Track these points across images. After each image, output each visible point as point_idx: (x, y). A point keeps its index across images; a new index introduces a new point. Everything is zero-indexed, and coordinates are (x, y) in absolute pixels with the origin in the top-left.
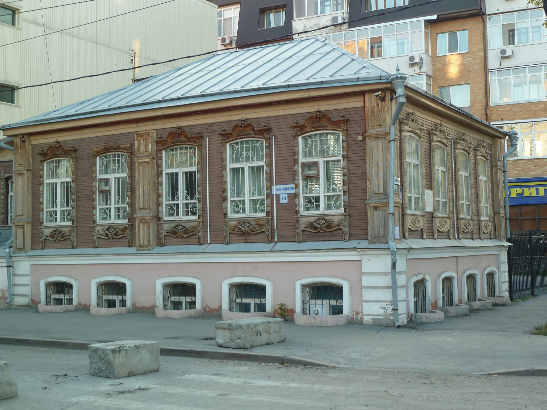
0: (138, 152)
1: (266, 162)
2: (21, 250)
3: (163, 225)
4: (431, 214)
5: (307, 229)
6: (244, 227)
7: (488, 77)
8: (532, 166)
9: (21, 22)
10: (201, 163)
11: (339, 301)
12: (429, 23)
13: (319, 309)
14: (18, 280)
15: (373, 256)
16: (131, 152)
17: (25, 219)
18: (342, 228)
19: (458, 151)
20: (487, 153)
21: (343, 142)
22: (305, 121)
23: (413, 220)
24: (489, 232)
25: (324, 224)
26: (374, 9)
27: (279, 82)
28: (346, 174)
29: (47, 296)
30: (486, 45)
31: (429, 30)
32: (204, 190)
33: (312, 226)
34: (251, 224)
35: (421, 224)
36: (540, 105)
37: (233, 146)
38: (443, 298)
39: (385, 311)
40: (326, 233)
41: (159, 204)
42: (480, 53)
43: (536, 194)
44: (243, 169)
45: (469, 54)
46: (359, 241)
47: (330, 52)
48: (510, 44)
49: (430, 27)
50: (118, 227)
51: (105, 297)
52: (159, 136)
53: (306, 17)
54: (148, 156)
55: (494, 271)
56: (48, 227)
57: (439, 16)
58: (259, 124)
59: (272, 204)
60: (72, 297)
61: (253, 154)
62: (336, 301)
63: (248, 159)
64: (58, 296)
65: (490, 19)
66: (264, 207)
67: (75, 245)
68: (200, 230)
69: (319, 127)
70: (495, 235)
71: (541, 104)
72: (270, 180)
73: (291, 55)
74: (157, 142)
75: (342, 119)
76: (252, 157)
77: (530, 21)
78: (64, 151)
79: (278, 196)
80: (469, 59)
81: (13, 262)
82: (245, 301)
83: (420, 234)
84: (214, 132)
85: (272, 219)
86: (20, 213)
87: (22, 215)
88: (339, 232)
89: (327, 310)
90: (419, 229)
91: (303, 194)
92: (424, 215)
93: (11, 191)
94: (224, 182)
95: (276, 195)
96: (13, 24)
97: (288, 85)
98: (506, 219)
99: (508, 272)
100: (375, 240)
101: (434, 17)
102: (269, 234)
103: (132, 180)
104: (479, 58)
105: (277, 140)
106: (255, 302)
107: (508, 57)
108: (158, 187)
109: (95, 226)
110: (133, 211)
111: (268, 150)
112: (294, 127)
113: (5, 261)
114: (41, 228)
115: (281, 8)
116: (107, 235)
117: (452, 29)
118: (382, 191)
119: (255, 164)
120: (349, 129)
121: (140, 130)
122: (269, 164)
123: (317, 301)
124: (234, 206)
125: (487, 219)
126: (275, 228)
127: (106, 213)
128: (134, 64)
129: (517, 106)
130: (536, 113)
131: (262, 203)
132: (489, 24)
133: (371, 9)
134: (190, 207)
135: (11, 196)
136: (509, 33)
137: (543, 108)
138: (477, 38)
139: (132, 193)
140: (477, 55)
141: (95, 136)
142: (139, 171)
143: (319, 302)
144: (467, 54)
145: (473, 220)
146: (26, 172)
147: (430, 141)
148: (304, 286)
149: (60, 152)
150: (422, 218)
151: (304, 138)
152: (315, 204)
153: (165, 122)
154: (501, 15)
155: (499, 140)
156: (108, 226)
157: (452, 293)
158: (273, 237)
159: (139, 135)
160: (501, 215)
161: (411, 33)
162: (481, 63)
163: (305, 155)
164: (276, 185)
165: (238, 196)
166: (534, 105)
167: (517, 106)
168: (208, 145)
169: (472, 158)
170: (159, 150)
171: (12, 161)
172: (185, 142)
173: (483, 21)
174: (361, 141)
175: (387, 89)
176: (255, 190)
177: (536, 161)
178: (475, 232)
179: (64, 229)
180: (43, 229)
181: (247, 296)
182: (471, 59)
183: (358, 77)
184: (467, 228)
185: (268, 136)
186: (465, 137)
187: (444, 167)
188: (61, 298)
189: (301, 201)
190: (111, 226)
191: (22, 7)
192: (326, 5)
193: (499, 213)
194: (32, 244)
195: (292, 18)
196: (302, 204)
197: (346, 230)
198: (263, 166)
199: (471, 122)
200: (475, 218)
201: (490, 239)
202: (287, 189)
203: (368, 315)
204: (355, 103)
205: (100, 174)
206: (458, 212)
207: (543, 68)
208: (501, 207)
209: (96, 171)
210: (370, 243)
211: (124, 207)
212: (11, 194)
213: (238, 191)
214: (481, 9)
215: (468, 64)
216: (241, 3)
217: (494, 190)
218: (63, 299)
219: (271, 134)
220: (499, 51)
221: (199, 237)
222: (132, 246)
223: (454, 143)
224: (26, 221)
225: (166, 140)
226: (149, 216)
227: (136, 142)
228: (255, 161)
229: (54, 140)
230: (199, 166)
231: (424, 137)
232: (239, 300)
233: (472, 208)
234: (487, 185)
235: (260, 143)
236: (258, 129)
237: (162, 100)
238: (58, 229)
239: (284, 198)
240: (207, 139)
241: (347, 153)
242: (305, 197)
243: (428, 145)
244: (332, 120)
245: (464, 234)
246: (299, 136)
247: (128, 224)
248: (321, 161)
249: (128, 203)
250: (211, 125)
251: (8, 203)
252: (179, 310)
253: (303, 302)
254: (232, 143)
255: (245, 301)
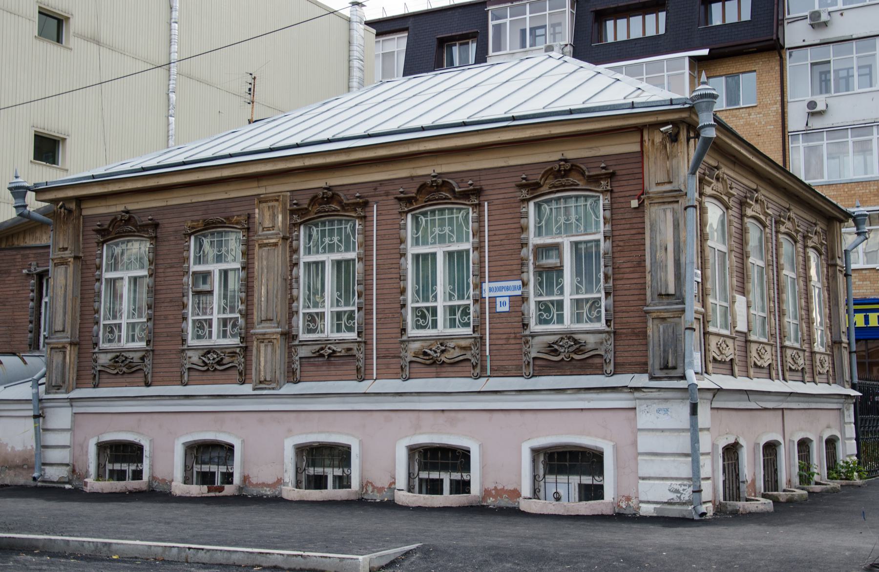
0: (261, 229)
1: (473, 243)
2: (58, 389)
3: (298, 347)
4: (744, 335)
5: (541, 355)
6: (435, 352)
7: (787, 143)
8: (857, 280)
9: (72, 39)
10: (364, 245)
11: (597, 478)
12: (696, 62)
13: (562, 491)
14: (51, 439)
15: (656, 401)
16: (248, 229)
17: (68, 338)
18: (603, 353)
19: (780, 236)
20: (822, 244)
21: (604, 210)
22: (540, 176)
23: (719, 343)
24: (825, 371)
25: (572, 345)
26: (610, 39)
27: (498, 112)
28: (610, 263)
29: (99, 465)
30: (785, 95)
31: (696, 72)
32: (368, 288)
33: (552, 349)
34: (446, 346)
35: (730, 352)
36: (870, 187)
37: (417, 218)
38: (724, 482)
39: (677, 496)
40: (574, 362)
41: (292, 314)
42: (775, 106)
43: (865, 324)
44: (434, 255)
45: (757, 108)
46: (632, 375)
47: (574, 71)
48: (821, 93)
49: (697, 67)
50: (223, 350)
51: (197, 468)
52: (295, 202)
53: (508, 51)
54: (276, 234)
55: (835, 436)
56: (106, 351)
57: (713, 51)
58: (462, 181)
59: (483, 313)
60: (141, 468)
61: (452, 231)
62: (591, 478)
63: (442, 239)
64: (117, 467)
65: (790, 55)
66: (469, 319)
67: (150, 380)
68: (361, 355)
69: (564, 186)
70: (834, 377)
71: (872, 185)
72: (480, 275)
73: (510, 78)
74: (292, 212)
75: (604, 171)
76: (450, 236)
77: (855, 58)
78: (135, 226)
79: (493, 300)
80: (758, 116)
81: (45, 410)
82: (435, 475)
83: (730, 368)
84: (387, 194)
85: (482, 338)
86: (59, 327)
87: (63, 331)
88: (597, 361)
89: (575, 493)
90: (728, 359)
91: (535, 296)
92: (734, 335)
93: (47, 295)
94: (402, 278)
95: (489, 297)
96: (59, 40)
97: (513, 116)
98: (850, 353)
99: (856, 440)
100: (659, 374)
101: (705, 52)
102: (477, 364)
103: (248, 273)
104: (774, 114)
105: (492, 208)
106: (452, 478)
107: (821, 113)
108: (291, 284)
109: (183, 351)
110: (249, 324)
111: (476, 225)
112: (521, 187)
113: (31, 407)
114: (94, 353)
115: (469, 38)
116: (205, 364)
117: (731, 70)
118: (671, 290)
119: (454, 248)
120: (615, 190)
121: (264, 192)
122: (478, 248)
123: (558, 477)
124: (418, 316)
125: (822, 350)
126: (488, 353)
127: (202, 326)
128: (252, 96)
129: (833, 188)
130: (864, 199)
131: (465, 311)
132: (789, 64)
133: (606, 40)
134: (344, 318)
135: (46, 303)
136: (821, 78)
137: (875, 190)
138: (770, 84)
139: (247, 296)
140: (771, 109)
141: (190, 202)
142: (262, 260)
143: (563, 478)
144: (754, 109)
145: (804, 351)
146: (72, 260)
147: (742, 216)
148: (536, 452)
149: (130, 227)
150: (731, 341)
151: (538, 206)
152: (555, 313)
153: (304, 180)
154: (809, 48)
155: (838, 224)
156: (206, 349)
157: (777, 469)
158: (483, 368)
159: (261, 200)
160: (844, 345)
161: (668, 76)
162: (776, 121)
163: (539, 232)
164: (489, 282)
165: (426, 299)
166: (860, 186)
167: (833, 188)
168: (377, 216)
169: (801, 250)
170: (294, 225)
171: (48, 247)
172: (338, 211)
173: (781, 57)
174: (635, 208)
175: (683, 121)
176: (453, 290)
177: (864, 272)
178: (807, 370)
179: (131, 355)
180: (97, 355)
181: (434, 467)
182: (761, 115)
183: (633, 102)
184: (795, 363)
185: (476, 202)
186: (792, 215)
187: (762, 259)
188: (123, 468)
189: (532, 307)
190: (212, 349)
191: (74, 13)
192: (537, 34)
193: (841, 342)
194: (77, 379)
195: (487, 52)
196: (534, 314)
197: (610, 357)
198: (468, 251)
199: (801, 190)
200: (806, 346)
201: (828, 383)
202: (508, 288)
203: (648, 502)
204: (627, 146)
205: (195, 264)
206: (782, 335)
207: (875, 129)
208: (843, 332)
209: (188, 258)
210: (652, 378)
211: (234, 318)
212: (45, 299)
213: (426, 289)
214: (778, 39)
215: (756, 124)
216: (410, 30)
217: (831, 305)
218: (126, 471)
219: (482, 198)
220: (806, 103)
221: (359, 367)
222: (246, 382)
223: (776, 222)
224: (69, 340)
225: (306, 209)
226: (277, 333)
227: (257, 211)
228: (454, 242)
229: (121, 208)
230: (362, 251)
231: (734, 209)
232: (424, 475)
233: (802, 330)
234: (822, 295)
235: (463, 214)
236: (460, 190)
237: (301, 144)
238: (123, 354)
239: (504, 304)
240: (375, 206)
241: (612, 228)
242: (538, 303)
243: (739, 221)
244: (587, 173)
245: (792, 373)
246: (528, 200)
247: (241, 345)
248: (566, 242)
249: (240, 312)
250: (381, 183)
251: (40, 314)
252: (323, 491)
253: (535, 478)
254: (416, 213)
255: (435, 475)
